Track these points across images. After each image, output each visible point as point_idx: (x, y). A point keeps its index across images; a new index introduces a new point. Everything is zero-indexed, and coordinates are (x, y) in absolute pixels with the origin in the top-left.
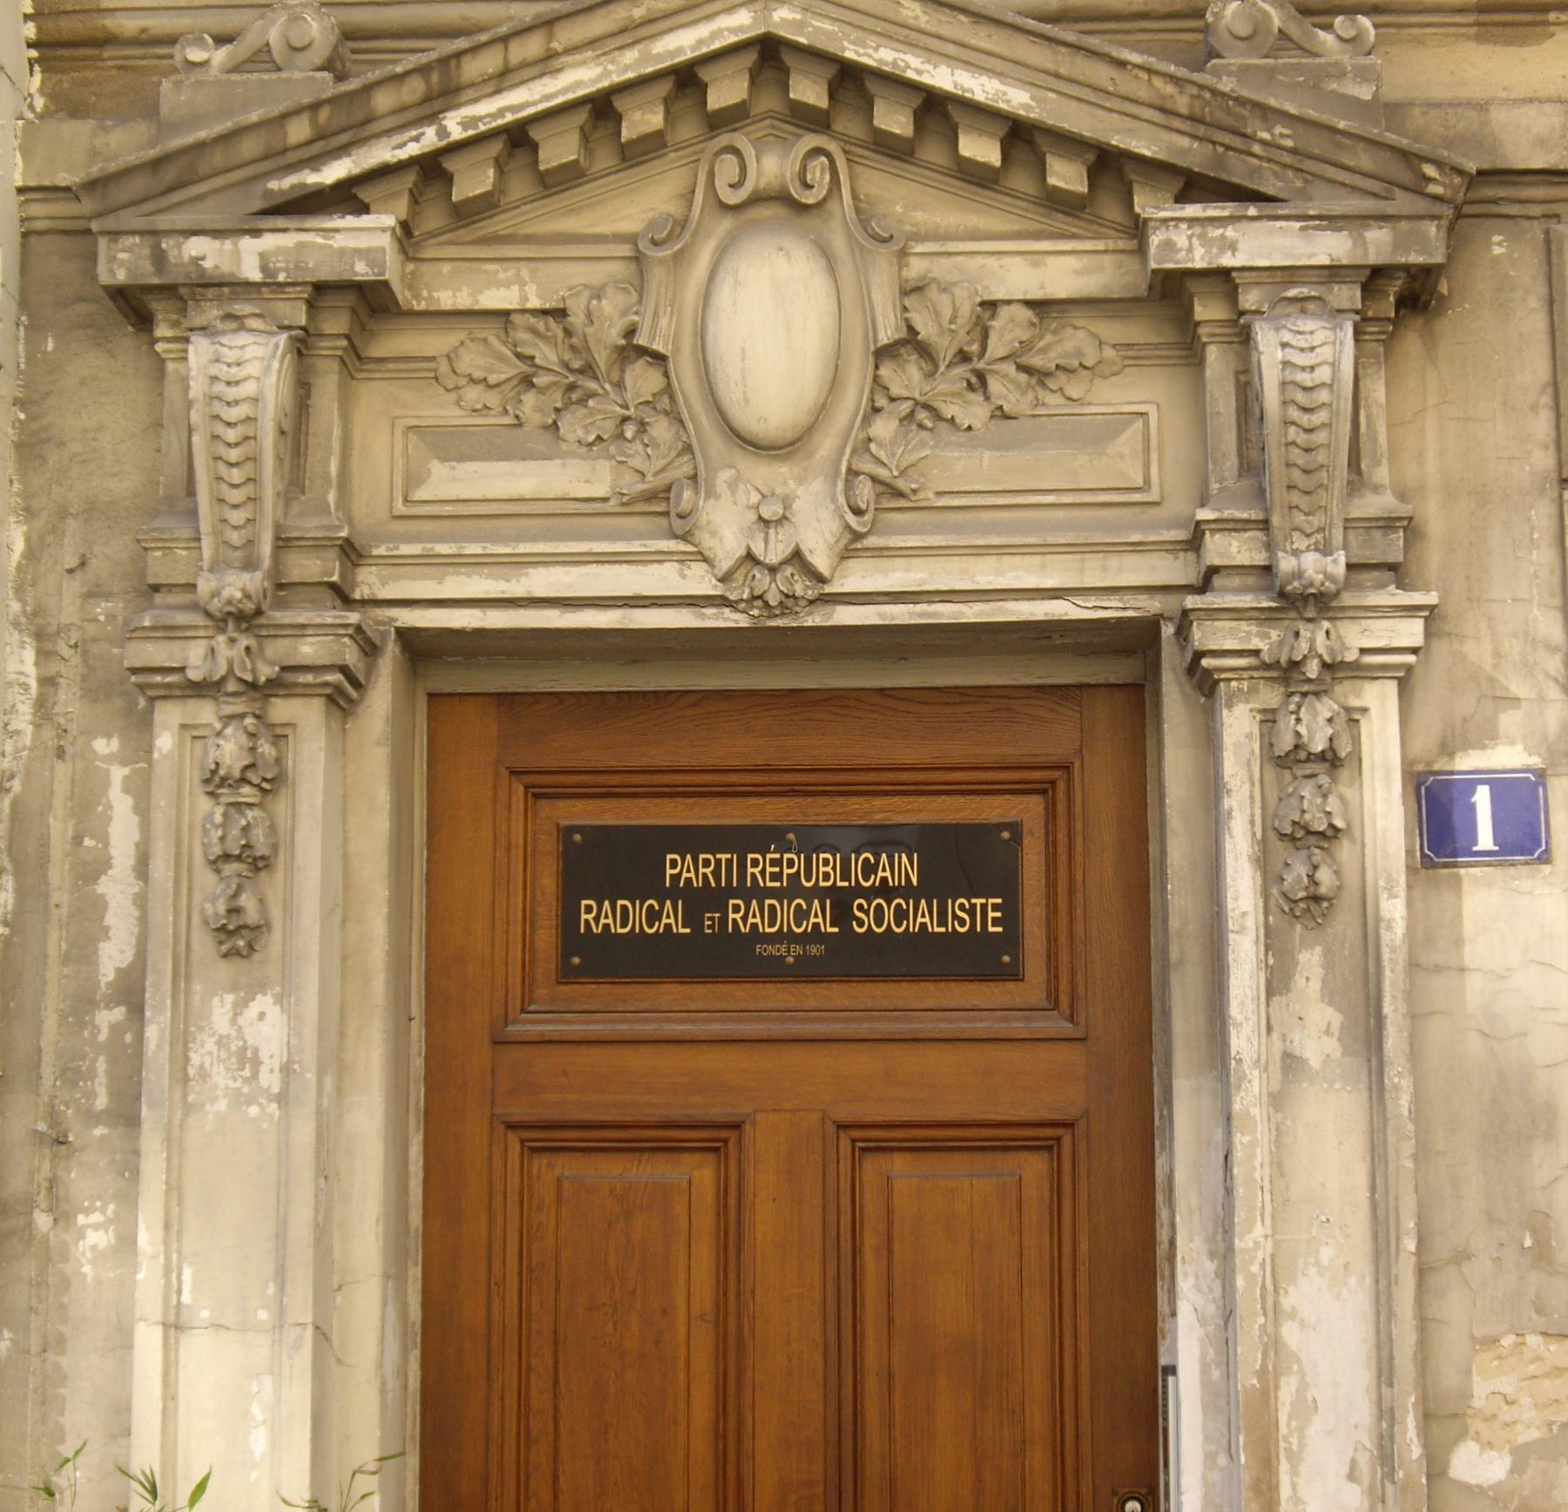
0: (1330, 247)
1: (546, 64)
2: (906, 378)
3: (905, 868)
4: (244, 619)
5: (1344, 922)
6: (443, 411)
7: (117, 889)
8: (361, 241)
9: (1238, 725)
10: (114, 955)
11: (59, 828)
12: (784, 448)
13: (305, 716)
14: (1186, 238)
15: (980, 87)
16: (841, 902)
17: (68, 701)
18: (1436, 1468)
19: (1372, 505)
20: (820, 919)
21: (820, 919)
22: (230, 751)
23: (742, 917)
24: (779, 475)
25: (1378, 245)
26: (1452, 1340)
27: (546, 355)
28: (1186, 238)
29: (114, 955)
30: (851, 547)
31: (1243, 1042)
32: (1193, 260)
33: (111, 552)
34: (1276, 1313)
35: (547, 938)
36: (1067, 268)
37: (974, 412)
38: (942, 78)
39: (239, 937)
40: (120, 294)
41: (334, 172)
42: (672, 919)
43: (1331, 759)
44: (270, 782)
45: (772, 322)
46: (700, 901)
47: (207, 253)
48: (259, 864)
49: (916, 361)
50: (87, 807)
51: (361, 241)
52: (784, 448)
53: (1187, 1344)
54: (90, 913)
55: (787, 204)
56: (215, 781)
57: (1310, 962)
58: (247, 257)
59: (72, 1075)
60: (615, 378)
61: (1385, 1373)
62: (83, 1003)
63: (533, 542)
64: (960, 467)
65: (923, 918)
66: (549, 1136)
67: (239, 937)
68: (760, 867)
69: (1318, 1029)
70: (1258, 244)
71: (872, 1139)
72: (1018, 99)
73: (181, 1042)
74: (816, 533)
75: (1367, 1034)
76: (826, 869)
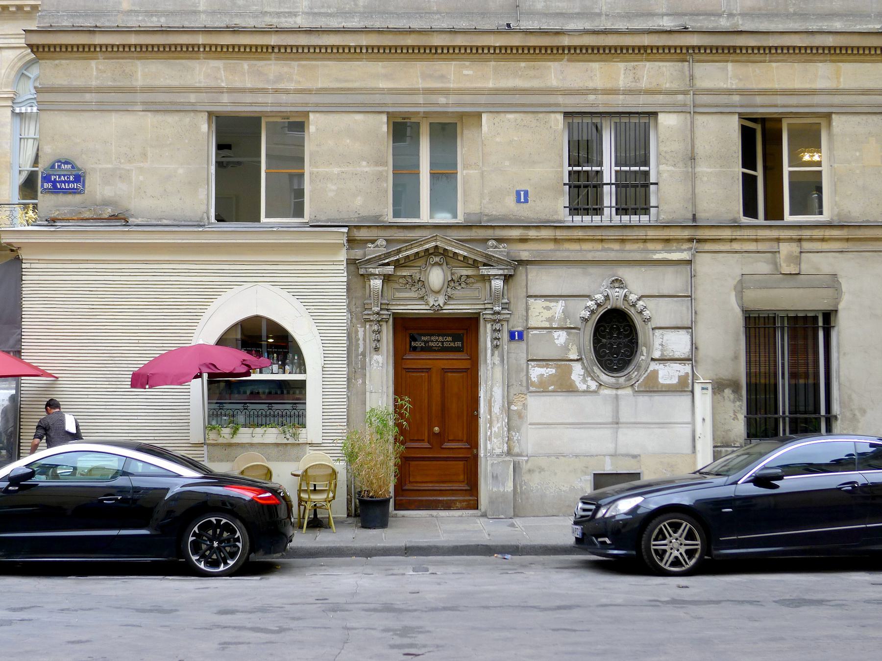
0: (501, 272)
1: (411, 248)
2: (452, 284)
3: (450, 339)
4: (378, 313)
5: (500, 348)
6: (397, 286)
7: (361, 342)
8: (390, 269)
9: (489, 326)
10: (361, 350)
11: (354, 335)
12: (438, 292)
13: (384, 324)
14: (484, 271)
15: (461, 252)
16: (442, 342)
17: (354, 320)
18: (509, 408)
19: (506, 301)
20: (440, 344)
21: (440, 344)
22: (376, 328)
23: (431, 344)
24: (437, 296)
25: (506, 272)
26: (511, 394)
27: (410, 280)
28: (484, 271)
29: (361, 350)
30: (445, 304)
31: (489, 361)
32: (465, 167)
33: (359, 303)
34: (492, 391)
35: (408, 347)
36: (469, 272)
37: (459, 288)
38: (457, 251)
39: (377, 349)
40: (362, 275)
41: (387, 261)
42: (423, 344)
43: (499, 330)
44: (379, 332)
45: (436, 277)
46: (426, 342)
47: (372, 271)
48: (378, 341)
49: (453, 282)
50: (357, 332)
51: (390, 269)
52: (438, 292)
53: (482, 394)
54: (357, 345)
55: (437, 264)
56: (374, 331)
57: (496, 352)
58: (377, 271)
59: (356, 364)
60: (420, 283)
61: (503, 398)
62: (357, 355)
63: (412, 305)
64: (458, 293)
65: (452, 344)
66: (408, 370)
67: (377, 349)
68: (433, 338)
69: (497, 360)
70: (493, 272)
71: (445, 371)
72: (465, 254)
73: (370, 361)
74: (441, 300)
75: (502, 361)
76: (441, 339)
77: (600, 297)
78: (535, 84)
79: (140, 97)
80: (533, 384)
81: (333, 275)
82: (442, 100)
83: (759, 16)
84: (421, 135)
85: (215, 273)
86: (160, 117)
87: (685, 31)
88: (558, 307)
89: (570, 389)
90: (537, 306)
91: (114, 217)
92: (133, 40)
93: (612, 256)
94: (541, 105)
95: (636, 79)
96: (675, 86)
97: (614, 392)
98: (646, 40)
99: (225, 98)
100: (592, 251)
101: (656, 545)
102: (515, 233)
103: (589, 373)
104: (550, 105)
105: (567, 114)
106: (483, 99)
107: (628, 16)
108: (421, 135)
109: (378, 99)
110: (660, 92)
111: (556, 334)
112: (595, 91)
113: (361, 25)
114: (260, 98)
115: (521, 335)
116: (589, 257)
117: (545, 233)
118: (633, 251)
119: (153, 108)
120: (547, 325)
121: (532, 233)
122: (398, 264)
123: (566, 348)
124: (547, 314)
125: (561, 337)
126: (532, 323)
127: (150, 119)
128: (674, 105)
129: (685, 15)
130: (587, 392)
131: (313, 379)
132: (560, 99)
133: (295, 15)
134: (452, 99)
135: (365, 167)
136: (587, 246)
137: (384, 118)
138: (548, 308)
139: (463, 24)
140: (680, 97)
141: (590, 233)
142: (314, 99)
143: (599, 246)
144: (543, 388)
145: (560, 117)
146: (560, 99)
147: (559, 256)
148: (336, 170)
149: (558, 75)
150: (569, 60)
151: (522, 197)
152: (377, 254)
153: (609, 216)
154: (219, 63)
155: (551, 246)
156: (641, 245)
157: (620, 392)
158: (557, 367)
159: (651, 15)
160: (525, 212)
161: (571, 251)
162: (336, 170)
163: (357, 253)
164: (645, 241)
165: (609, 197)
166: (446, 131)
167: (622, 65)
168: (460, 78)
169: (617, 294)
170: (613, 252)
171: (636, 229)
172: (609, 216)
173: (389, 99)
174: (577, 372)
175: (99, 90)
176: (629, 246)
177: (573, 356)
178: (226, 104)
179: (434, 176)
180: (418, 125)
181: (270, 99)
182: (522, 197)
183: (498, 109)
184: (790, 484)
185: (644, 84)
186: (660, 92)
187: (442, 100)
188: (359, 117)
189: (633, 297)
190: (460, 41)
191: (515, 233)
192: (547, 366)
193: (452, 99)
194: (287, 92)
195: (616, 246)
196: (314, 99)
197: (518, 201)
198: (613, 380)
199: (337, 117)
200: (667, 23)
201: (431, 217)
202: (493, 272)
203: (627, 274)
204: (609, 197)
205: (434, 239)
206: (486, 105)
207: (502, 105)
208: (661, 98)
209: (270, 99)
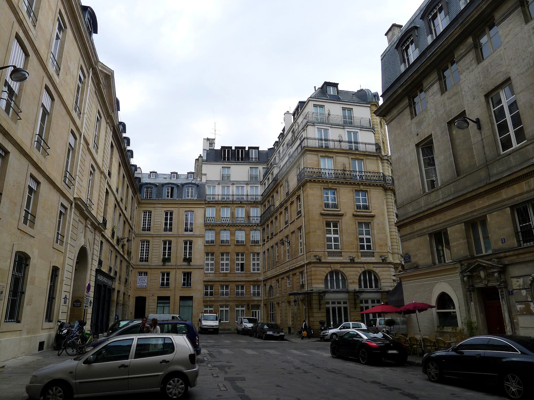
78: (499, 199)
80: (518, 311)
81: (456, 278)
82: (475, 214)
84: (475, 225)
85: (433, 280)
88: (521, 280)
90: (514, 280)
91: (416, 267)
92: (411, 219)
94: (502, 206)
99: (430, 229)
101: (509, 376)
102: (502, 255)
105: (510, 207)
106: (485, 210)
107: (521, 164)
108: (475, 225)
111: (522, 291)
113: (471, 189)
114: (437, 227)
115: (512, 292)
116: (527, 259)
117: (511, 253)
119: (419, 236)
120: (518, 288)
121: (507, 254)
122: (470, 271)
124: (518, 284)
125: (524, 292)
126: (514, 288)
131: (457, 310)
132: (507, 202)
133: (439, 200)
134: (478, 212)
135: (462, 241)
136: (527, 255)
137: (463, 224)
138: (518, 281)
139: (476, 187)
141: (527, 250)
142: (447, 223)
146: (507, 202)
150: (507, 187)
151: (503, 241)
152: (470, 269)
154: (428, 220)
155: (515, 257)
158: (525, 304)
160: (505, 246)
161: (522, 258)
166: (483, 221)
167: (524, 183)
171: (6, 333)
175: (409, 234)
177: (530, 300)
178: (431, 230)
179: (484, 238)
181: (438, 226)
182: (503, 241)
183: (491, 212)
184: (467, 352)
187: (475, 214)
188: (458, 226)
191: (502, 255)
193: (478, 212)
196: (447, 223)
197: (502, 243)
199: (453, 227)
201: (486, 252)
202: (495, 270)
205: (477, 261)
206: (487, 211)
209: (438, 226)
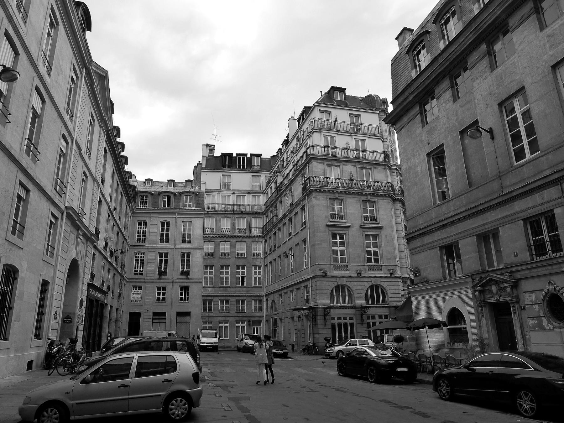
55: (493, 284)
67: (483, 316)
77: (546, 290)
78: (512, 212)
79: (426, 247)
80: (530, 327)
83: (537, 174)
86: (431, 251)
87: (555, 173)
88: (534, 295)
89: (543, 329)
91: (426, 281)
92: (421, 232)
93: (547, 272)
94: (515, 219)
95: (543, 198)
96: (558, 196)
97: (559, 330)
98: (539, 183)
100: (541, 271)
101: (522, 394)
103: (549, 322)
104: (517, 218)
105: (523, 220)
106: (498, 223)
107: (535, 175)
108: (487, 238)
109: (472, 231)
110: (551, 201)
111: (535, 306)
112: (529, 208)
115: (524, 307)
117: (524, 267)
118: (556, 269)
121: (520, 268)
123: (539, 312)
124: (530, 299)
125: (536, 308)
126: (526, 303)
127: (429, 252)
128: (558, 204)
129: (554, 166)
130: (550, 330)
131: (468, 326)
132: (520, 215)
134: (490, 225)
136: (540, 269)
137: (475, 237)
138: (530, 296)
139: (488, 199)
140: (560, 200)
141: (540, 264)
143: (544, 269)
144: (534, 329)
145: (522, 221)
147: (530, 275)
148: (467, 257)
149: (519, 206)
151: (516, 255)
153: (550, 254)
154: (438, 232)
155: (528, 271)
156: (558, 266)
157: (562, 330)
158: (537, 320)
159: (542, 171)
161: (535, 272)
162: (467, 257)
163: (320, 314)
164: (559, 263)
165: (549, 248)
166: (495, 234)
167: (537, 195)
168: (492, 216)
169: (551, 287)
170: (549, 270)
172: (550, 254)
173: (475, 231)
174: (545, 321)
176: (554, 267)
178: (441, 243)
180: (489, 236)
183: (503, 225)
185: (546, 199)
186: (551, 201)
188: (469, 238)
189: (558, 289)
190: (486, 206)
192: (534, 320)
193: (490, 225)
194: (452, 236)
195: (550, 268)
196: (458, 236)
198: (558, 325)
200: (548, 172)
203: (554, 279)
204: (549, 248)
207: (503, 223)
208: (553, 203)
